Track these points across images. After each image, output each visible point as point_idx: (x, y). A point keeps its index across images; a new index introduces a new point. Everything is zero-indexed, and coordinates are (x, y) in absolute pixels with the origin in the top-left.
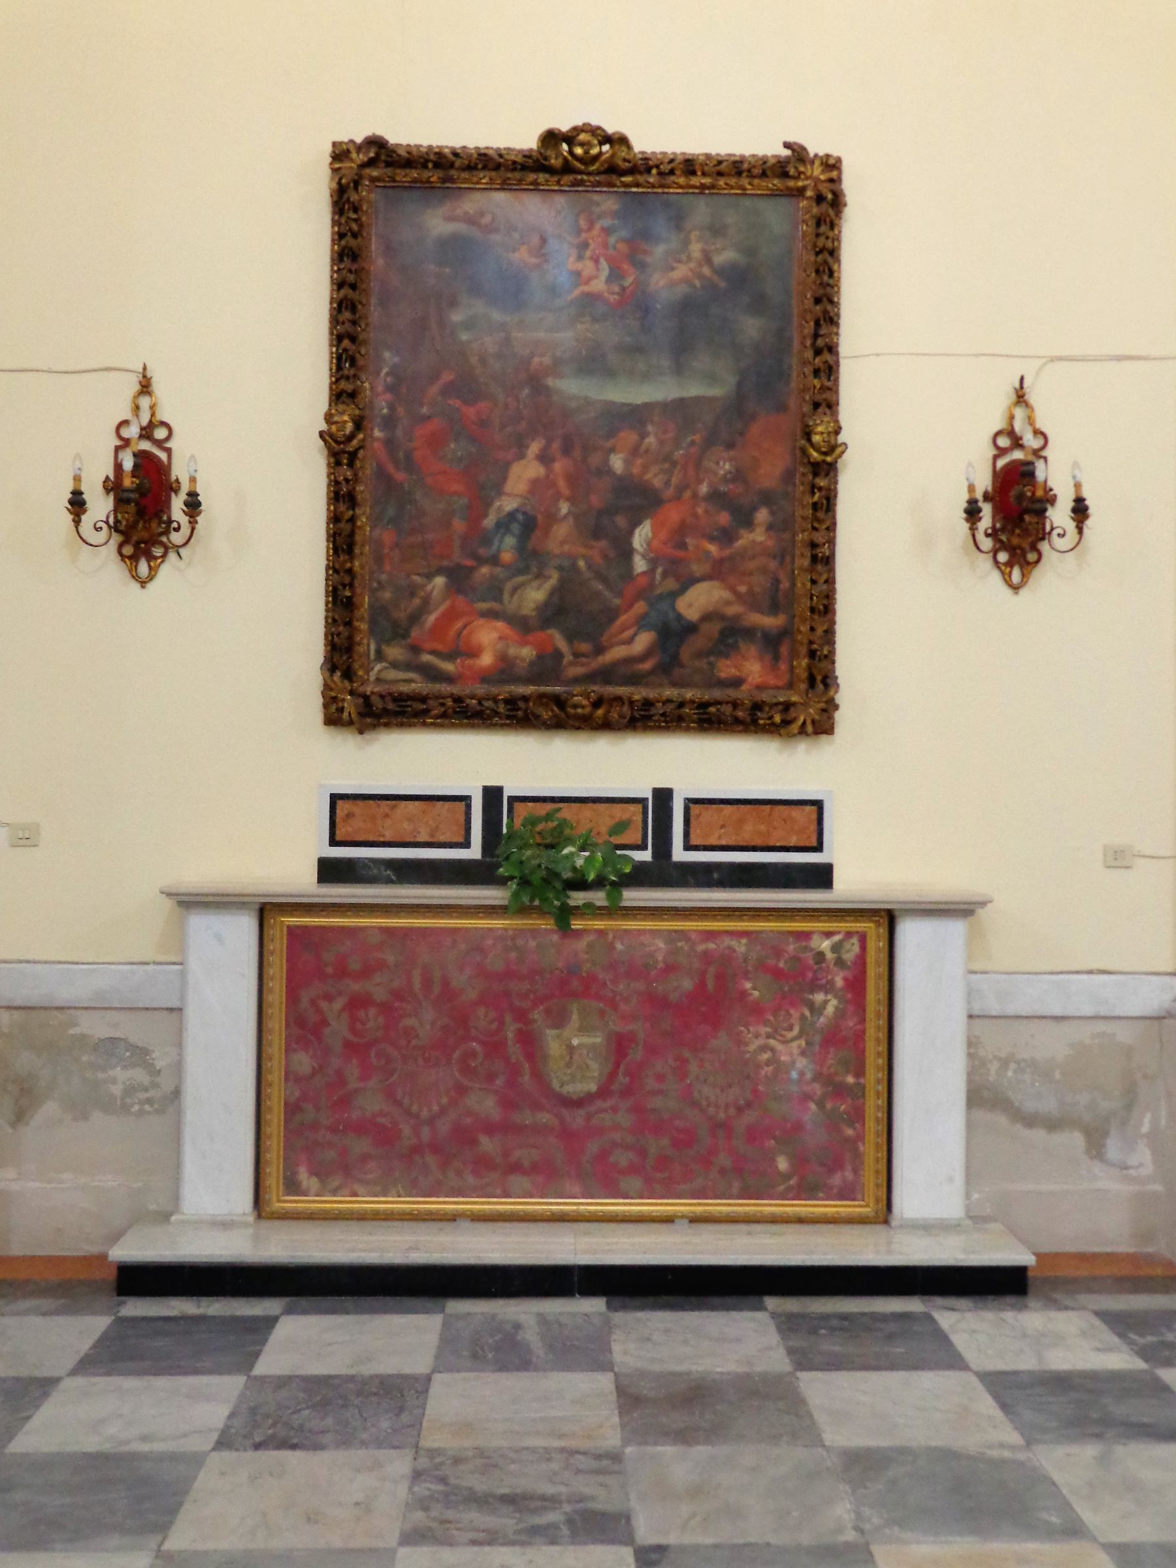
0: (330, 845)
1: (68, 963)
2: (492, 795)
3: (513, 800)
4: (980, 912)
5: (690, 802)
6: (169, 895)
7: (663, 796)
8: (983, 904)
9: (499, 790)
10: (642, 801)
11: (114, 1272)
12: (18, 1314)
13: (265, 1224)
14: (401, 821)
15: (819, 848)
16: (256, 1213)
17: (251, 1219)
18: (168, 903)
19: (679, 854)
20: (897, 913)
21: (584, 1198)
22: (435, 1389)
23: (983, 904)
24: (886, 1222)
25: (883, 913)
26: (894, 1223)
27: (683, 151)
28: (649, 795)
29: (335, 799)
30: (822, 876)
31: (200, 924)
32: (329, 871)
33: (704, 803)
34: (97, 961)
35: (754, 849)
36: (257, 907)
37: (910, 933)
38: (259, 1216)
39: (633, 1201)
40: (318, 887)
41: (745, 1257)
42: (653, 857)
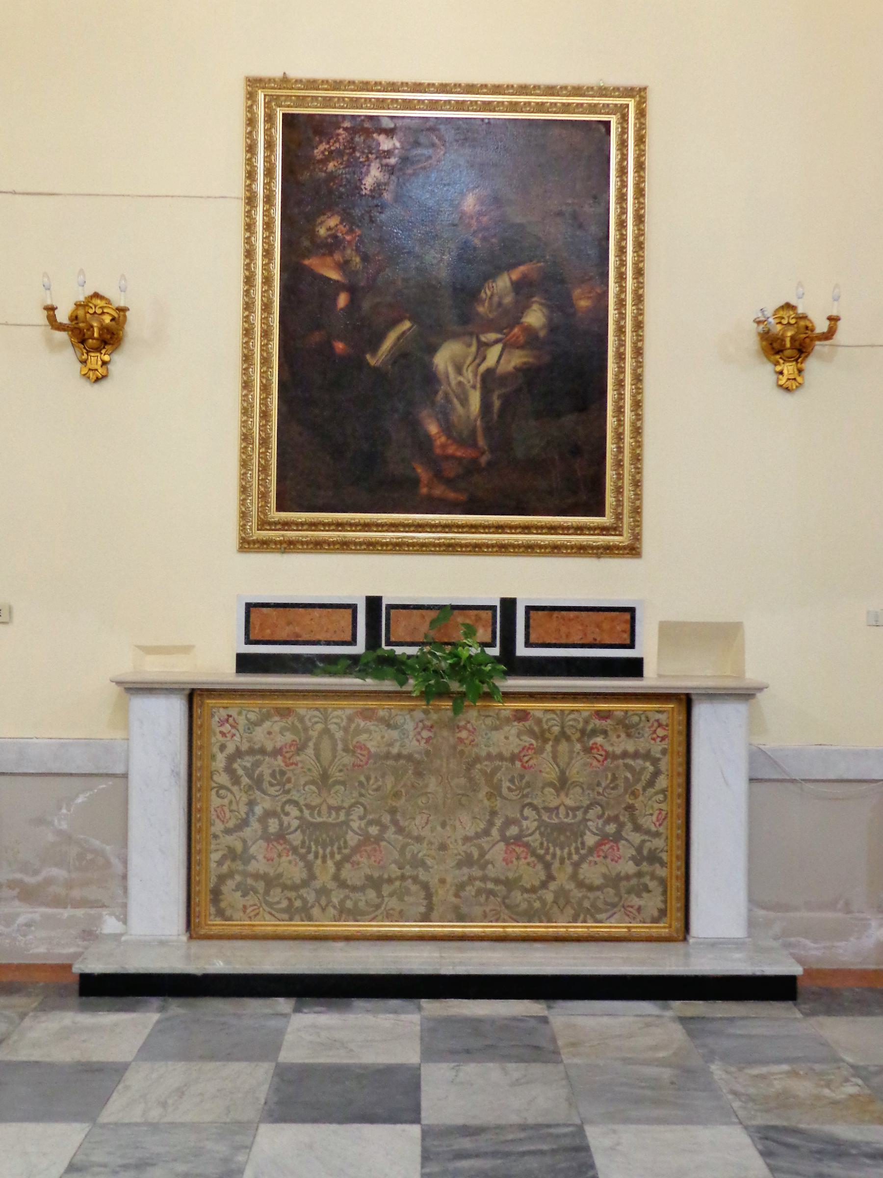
0: (246, 644)
1: (27, 738)
2: (373, 603)
3: (390, 607)
4: (759, 695)
5: (529, 609)
6: (119, 683)
7: (509, 605)
8: (760, 689)
9: (379, 599)
10: (493, 608)
11: (78, 978)
12: (315, 1013)
13: (195, 944)
14: (309, 622)
15: (632, 646)
16: (188, 935)
17: (184, 938)
18: (117, 689)
19: (522, 650)
20: (693, 697)
21: (457, 922)
22: (422, 1068)
23: (760, 689)
24: (685, 939)
25: (683, 697)
26: (691, 941)
27: (440, 82)
28: (498, 604)
29: (249, 606)
30: (634, 668)
31: (142, 705)
32: (245, 663)
33: (353, 624)
34: (23, 736)
35: (582, 646)
36: (187, 692)
37: (701, 712)
38: (191, 937)
39: (435, 924)
40: (237, 676)
41: (464, 968)
42: (501, 652)
